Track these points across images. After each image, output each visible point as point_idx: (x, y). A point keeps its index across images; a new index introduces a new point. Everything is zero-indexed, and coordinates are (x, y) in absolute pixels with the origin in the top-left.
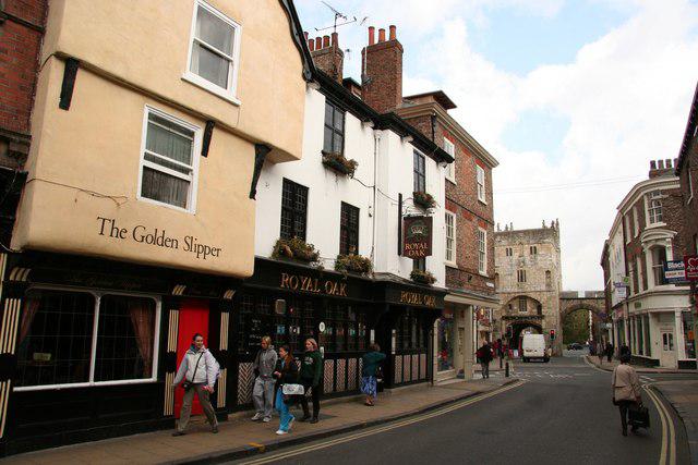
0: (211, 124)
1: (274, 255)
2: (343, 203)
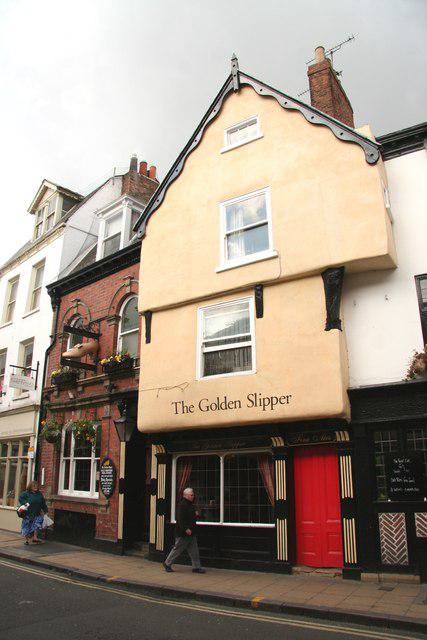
0: (258, 289)
1: (411, 375)
2: (33, 338)
